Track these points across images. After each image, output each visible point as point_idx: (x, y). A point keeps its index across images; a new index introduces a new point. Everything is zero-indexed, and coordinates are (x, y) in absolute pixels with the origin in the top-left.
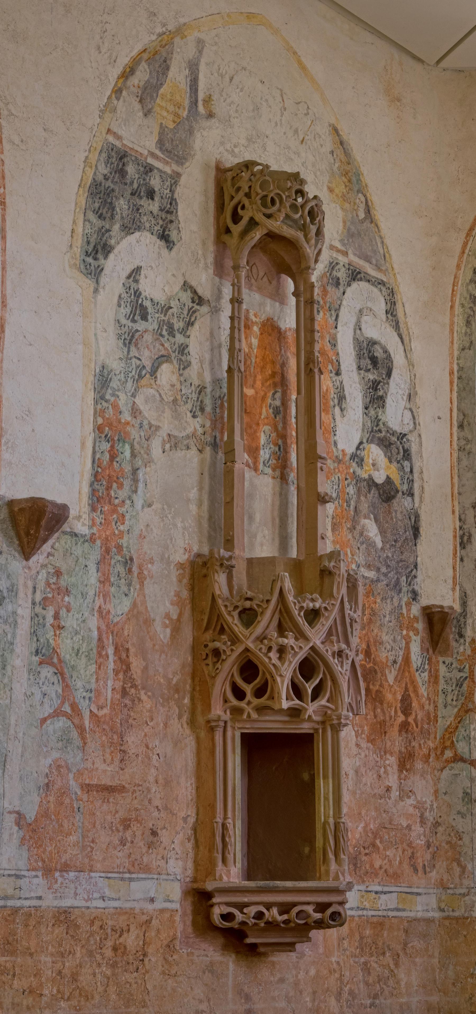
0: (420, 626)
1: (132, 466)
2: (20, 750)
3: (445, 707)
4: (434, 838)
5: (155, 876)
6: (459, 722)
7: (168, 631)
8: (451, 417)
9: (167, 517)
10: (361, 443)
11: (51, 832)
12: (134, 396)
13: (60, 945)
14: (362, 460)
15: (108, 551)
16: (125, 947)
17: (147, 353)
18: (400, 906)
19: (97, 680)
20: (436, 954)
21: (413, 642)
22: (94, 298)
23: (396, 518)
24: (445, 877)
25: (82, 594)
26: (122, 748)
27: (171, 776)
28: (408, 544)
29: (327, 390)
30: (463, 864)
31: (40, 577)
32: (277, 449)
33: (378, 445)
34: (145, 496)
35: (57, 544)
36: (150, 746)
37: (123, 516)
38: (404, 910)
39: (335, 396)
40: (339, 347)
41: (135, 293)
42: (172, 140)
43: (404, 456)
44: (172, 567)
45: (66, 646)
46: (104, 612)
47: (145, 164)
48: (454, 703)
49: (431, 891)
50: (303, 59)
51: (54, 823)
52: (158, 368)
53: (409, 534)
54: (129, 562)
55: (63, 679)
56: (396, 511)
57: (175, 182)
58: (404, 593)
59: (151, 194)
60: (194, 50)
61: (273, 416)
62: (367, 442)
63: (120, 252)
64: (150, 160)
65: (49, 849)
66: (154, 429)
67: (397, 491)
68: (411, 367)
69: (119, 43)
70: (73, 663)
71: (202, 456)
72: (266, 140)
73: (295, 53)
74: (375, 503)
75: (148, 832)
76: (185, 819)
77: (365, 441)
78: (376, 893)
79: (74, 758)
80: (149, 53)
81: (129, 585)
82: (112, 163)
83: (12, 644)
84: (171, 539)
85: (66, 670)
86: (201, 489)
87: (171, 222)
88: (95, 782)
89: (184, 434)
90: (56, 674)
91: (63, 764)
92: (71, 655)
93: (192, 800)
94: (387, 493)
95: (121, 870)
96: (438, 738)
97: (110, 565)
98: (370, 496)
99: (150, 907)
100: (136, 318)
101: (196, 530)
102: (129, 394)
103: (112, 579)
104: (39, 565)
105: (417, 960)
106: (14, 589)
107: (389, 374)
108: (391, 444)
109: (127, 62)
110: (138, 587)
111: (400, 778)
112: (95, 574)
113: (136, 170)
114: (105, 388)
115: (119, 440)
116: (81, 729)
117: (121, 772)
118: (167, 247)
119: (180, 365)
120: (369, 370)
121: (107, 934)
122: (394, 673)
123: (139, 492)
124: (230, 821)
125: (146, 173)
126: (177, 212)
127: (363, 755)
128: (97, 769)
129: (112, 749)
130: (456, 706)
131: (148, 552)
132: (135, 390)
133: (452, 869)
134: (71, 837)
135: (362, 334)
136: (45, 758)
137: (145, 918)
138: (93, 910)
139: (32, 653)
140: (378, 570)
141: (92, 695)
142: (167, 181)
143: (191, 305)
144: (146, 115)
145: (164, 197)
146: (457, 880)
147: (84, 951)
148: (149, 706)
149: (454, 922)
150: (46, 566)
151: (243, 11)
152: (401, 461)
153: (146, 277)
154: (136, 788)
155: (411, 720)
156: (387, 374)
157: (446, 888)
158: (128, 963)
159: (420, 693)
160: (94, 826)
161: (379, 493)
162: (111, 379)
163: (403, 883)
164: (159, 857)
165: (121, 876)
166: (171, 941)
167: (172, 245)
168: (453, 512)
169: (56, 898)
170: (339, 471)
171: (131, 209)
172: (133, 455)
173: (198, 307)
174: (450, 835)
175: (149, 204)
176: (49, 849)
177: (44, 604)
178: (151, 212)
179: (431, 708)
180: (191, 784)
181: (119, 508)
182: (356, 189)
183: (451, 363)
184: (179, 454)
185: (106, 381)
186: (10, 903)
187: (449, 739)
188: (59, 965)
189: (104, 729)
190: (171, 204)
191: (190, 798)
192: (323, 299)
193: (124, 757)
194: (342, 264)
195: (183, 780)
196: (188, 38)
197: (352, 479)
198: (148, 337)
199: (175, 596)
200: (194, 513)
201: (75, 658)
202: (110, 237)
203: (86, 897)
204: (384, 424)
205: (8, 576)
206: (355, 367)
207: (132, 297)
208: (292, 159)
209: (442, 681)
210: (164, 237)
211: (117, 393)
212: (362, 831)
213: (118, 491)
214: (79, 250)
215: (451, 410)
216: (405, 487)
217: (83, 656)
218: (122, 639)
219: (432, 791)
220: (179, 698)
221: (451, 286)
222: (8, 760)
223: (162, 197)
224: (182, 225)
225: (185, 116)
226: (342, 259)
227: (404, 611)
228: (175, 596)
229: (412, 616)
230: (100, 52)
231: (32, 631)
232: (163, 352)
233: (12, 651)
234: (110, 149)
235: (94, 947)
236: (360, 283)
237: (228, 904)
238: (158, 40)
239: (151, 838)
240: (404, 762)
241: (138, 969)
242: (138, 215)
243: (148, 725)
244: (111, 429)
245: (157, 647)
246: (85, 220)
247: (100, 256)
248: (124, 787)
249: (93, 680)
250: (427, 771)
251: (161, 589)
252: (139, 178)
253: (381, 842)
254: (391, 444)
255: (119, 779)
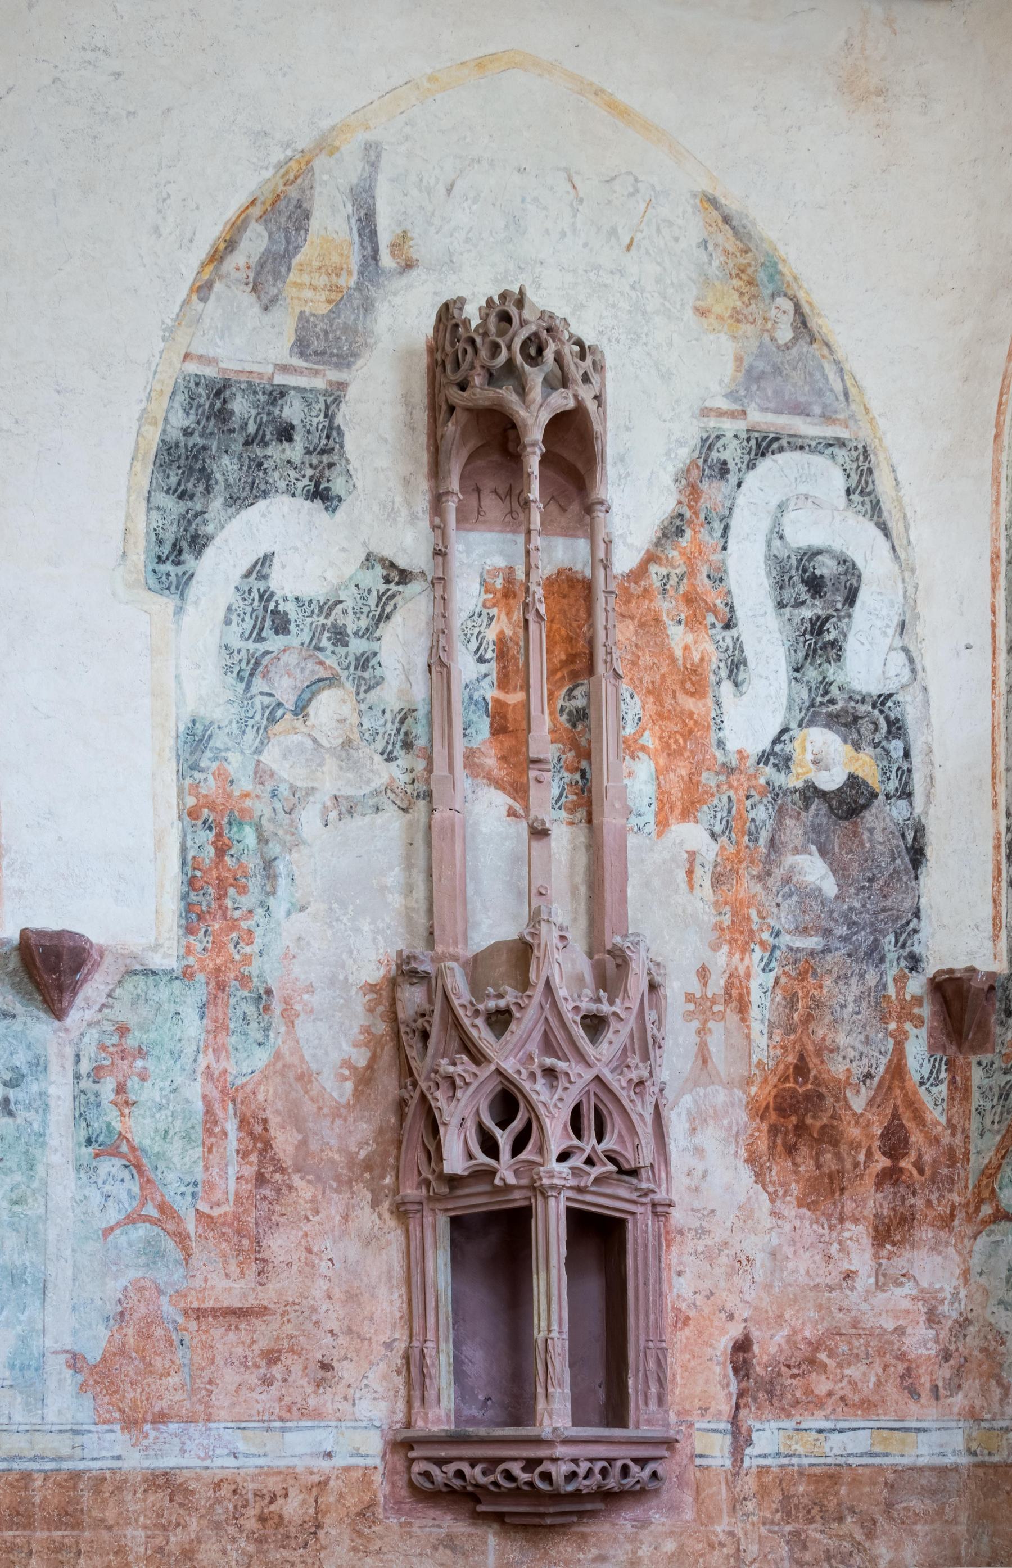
0: (926, 1011)
1: (262, 857)
2: (69, 1273)
3: (982, 1135)
4: (960, 1345)
5: (333, 1424)
6: (1003, 1158)
7: (349, 1086)
8: (994, 638)
9: (338, 920)
10: (785, 731)
11: (132, 1374)
12: (258, 751)
13: (159, 1515)
14: (788, 758)
15: (221, 986)
16: (281, 1517)
17: (286, 682)
18: (877, 1449)
19: (206, 1168)
20: (963, 1518)
21: (912, 1039)
22: (177, 622)
23: (871, 841)
24: (978, 1403)
25: (172, 1053)
26: (260, 1256)
27: (359, 1288)
28: (899, 880)
29: (702, 659)
30: (1005, 1382)
31: (86, 1040)
32: (577, 776)
33: (827, 726)
34: (293, 896)
35: (118, 991)
36: (315, 1249)
37: (250, 932)
38: (887, 1455)
39: (722, 665)
40: (733, 581)
41: (261, 597)
42: (326, 333)
43: (889, 732)
44: (353, 992)
45: (141, 1129)
46: (217, 1073)
47: (269, 388)
48: (996, 1126)
49: (954, 1424)
50: (621, 97)
51: (137, 1362)
52: (310, 700)
53: (903, 861)
54: (264, 997)
55: (141, 1172)
56: (871, 831)
57: (335, 400)
58: (891, 962)
59: (286, 433)
60: (360, 165)
61: (568, 726)
62: (800, 725)
63: (226, 541)
64: (280, 379)
65: (130, 1395)
66: (300, 796)
67: (874, 795)
68: (907, 574)
69: (197, 208)
70: (156, 1149)
71: (409, 816)
72: (538, 269)
73: (598, 92)
74: (819, 825)
75: (314, 1366)
76: (388, 1346)
77: (793, 725)
78: (820, 1431)
79: (170, 1275)
80: (264, 203)
81: (266, 1030)
82: (200, 406)
83: (42, 1135)
84: (351, 952)
85: (145, 1161)
86: (409, 867)
87: (331, 465)
88: (209, 1304)
89: (367, 790)
90: (126, 1167)
91: (149, 1284)
92: (153, 1139)
93: (401, 1318)
94: (851, 802)
95: (266, 1418)
96: (970, 1187)
97: (227, 1005)
98: (807, 817)
99: (326, 1465)
100: (264, 634)
101: (400, 930)
102: (247, 752)
103: (232, 1026)
104: (85, 1023)
105: (919, 1527)
106: (42, 1061)
107: (851, 599)
108: (856, 719)
109: (218, 234)
110: (283, 1029)
111: (876, 1256)
112: (197, 1022)
113: (252, 403)
114: (199, 753)
115: (230, 823)
116: (182, 1238)
117: (260, 1288)
118: (327, 509)
119: (358, 686)
120: (803, 603)
121: (247, 1501)
122: (865, 1094)
123: (279, 893)
124: (430, 1344)
125: (273, 402)
126: (342, 447)
127: (788, 1227)
128: (213, 1287)
129: (241, 1258)
130: (998, 1132)
131: (303, 977)
132: (262, 742)
133: (988, 1390)
134: (169, 1379)
135: (786, 545)
136: (116, 1278)
137: (316, 1478)
138: (217, 1471)
139: (79, 1144)
140: (827, 932)
141: (199, 1189)
142: (318, 402)
143: (383, 588)
144: (266, 309)
145: (313, 429)
146: (996, 1408)
147: (205, 1522)
148: (310, 1194)
149: (991, 1471)
150: (98, 1022)
151: (467, 58)
152: (884, 743)
153: (283, 567)
154: (288, 1308)
155: (905, 1164)
156: (846, 600)
157: (978, 1420)
158: (288, 1537)
159: (929, 1119)
160: (213, 1363)
161: (830, 807)
162: (210, 737)
163: (885, 1414)
164: (338, 1398)
165: (266, 1425)
166: (368, 1508)
167: (335, 502)
168: (995, 805)
169: (147, 1457)
170: (730, 787)
171: (245, 469)
172: (262, 840)
173: (400, 588)
174: (986, 1338)
175: (284, 451)
176: (130, 1395)
177: (96, 1075)
178: (289, 462)
179: (958, 1140)
180: (401, 1296)
181: (242, 923)
182: (767, 292)
183: (995, 540)
184: (358, 823)
185: (201, 741)
186: (66, 1465)
187: (987, 1186)
188: (160, 1541)
189: (224, 1234)
190: (328, 437)
191: (398, 1315)
192: (690, 507)
193: (264, 1267)
194: (730, 435)
195: (382, 1292)
196: (342, 149)
197: (763, 794)
198: (291, 659)
199: (361, 1033)
200: (397, 906)
201: (161, 1142)
202: (205, 522)
203: (202, 1455)
204: (840, 688)
205: (29, 1047)
206: (770, 605)
207: (256, 603)
208: (606, 286)
209: (976, 1094)
210: (321, 494)
211: (223, 754)
212: (783, 1342)
213: (238, 898)
214: (143, 557)
215: (994, 625)
216: (893, 785)
217: (176, 1138)
218: (253, 1107)
219: (958, 1271)
220: (372, 1178)
221: (996, 398)
222: (50, 1286)
223: (309, 432)
224: (354, 464)
225: (352, 284)
226: (729, 426)
227: (892, 991)
228: (361, 1033)
229: (908, 997)
230: (160, 236)
231: (77, 1114)
232: (322, 673)
233: (43, 1145)
234: (192, 385)
235: (223, 1517)
236: (778, 457)
237: (428, 1459)
238: (279, 174)
239: (321, 1373)
240: (889, 1230)
241: (306, 1544)
242: (261, 474)
243: (309, 1220)
244: (212, 809)
245: (326, 1110)
246: (149, 509)
247: (186, 556)
248: (266, 1308)
249: (199, 1168)
250: (947, 1243)
251: (330, 1027)
252: (259, 414)
253: (829, 1357)
254: (856, 719)
255: (256, 1299)
